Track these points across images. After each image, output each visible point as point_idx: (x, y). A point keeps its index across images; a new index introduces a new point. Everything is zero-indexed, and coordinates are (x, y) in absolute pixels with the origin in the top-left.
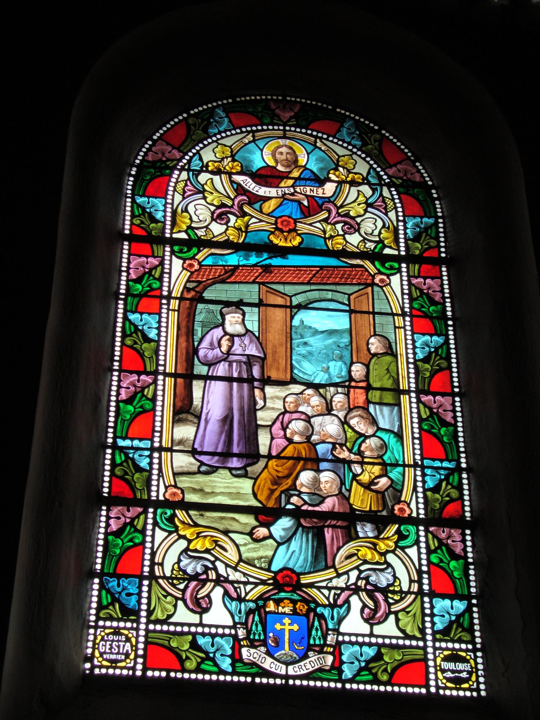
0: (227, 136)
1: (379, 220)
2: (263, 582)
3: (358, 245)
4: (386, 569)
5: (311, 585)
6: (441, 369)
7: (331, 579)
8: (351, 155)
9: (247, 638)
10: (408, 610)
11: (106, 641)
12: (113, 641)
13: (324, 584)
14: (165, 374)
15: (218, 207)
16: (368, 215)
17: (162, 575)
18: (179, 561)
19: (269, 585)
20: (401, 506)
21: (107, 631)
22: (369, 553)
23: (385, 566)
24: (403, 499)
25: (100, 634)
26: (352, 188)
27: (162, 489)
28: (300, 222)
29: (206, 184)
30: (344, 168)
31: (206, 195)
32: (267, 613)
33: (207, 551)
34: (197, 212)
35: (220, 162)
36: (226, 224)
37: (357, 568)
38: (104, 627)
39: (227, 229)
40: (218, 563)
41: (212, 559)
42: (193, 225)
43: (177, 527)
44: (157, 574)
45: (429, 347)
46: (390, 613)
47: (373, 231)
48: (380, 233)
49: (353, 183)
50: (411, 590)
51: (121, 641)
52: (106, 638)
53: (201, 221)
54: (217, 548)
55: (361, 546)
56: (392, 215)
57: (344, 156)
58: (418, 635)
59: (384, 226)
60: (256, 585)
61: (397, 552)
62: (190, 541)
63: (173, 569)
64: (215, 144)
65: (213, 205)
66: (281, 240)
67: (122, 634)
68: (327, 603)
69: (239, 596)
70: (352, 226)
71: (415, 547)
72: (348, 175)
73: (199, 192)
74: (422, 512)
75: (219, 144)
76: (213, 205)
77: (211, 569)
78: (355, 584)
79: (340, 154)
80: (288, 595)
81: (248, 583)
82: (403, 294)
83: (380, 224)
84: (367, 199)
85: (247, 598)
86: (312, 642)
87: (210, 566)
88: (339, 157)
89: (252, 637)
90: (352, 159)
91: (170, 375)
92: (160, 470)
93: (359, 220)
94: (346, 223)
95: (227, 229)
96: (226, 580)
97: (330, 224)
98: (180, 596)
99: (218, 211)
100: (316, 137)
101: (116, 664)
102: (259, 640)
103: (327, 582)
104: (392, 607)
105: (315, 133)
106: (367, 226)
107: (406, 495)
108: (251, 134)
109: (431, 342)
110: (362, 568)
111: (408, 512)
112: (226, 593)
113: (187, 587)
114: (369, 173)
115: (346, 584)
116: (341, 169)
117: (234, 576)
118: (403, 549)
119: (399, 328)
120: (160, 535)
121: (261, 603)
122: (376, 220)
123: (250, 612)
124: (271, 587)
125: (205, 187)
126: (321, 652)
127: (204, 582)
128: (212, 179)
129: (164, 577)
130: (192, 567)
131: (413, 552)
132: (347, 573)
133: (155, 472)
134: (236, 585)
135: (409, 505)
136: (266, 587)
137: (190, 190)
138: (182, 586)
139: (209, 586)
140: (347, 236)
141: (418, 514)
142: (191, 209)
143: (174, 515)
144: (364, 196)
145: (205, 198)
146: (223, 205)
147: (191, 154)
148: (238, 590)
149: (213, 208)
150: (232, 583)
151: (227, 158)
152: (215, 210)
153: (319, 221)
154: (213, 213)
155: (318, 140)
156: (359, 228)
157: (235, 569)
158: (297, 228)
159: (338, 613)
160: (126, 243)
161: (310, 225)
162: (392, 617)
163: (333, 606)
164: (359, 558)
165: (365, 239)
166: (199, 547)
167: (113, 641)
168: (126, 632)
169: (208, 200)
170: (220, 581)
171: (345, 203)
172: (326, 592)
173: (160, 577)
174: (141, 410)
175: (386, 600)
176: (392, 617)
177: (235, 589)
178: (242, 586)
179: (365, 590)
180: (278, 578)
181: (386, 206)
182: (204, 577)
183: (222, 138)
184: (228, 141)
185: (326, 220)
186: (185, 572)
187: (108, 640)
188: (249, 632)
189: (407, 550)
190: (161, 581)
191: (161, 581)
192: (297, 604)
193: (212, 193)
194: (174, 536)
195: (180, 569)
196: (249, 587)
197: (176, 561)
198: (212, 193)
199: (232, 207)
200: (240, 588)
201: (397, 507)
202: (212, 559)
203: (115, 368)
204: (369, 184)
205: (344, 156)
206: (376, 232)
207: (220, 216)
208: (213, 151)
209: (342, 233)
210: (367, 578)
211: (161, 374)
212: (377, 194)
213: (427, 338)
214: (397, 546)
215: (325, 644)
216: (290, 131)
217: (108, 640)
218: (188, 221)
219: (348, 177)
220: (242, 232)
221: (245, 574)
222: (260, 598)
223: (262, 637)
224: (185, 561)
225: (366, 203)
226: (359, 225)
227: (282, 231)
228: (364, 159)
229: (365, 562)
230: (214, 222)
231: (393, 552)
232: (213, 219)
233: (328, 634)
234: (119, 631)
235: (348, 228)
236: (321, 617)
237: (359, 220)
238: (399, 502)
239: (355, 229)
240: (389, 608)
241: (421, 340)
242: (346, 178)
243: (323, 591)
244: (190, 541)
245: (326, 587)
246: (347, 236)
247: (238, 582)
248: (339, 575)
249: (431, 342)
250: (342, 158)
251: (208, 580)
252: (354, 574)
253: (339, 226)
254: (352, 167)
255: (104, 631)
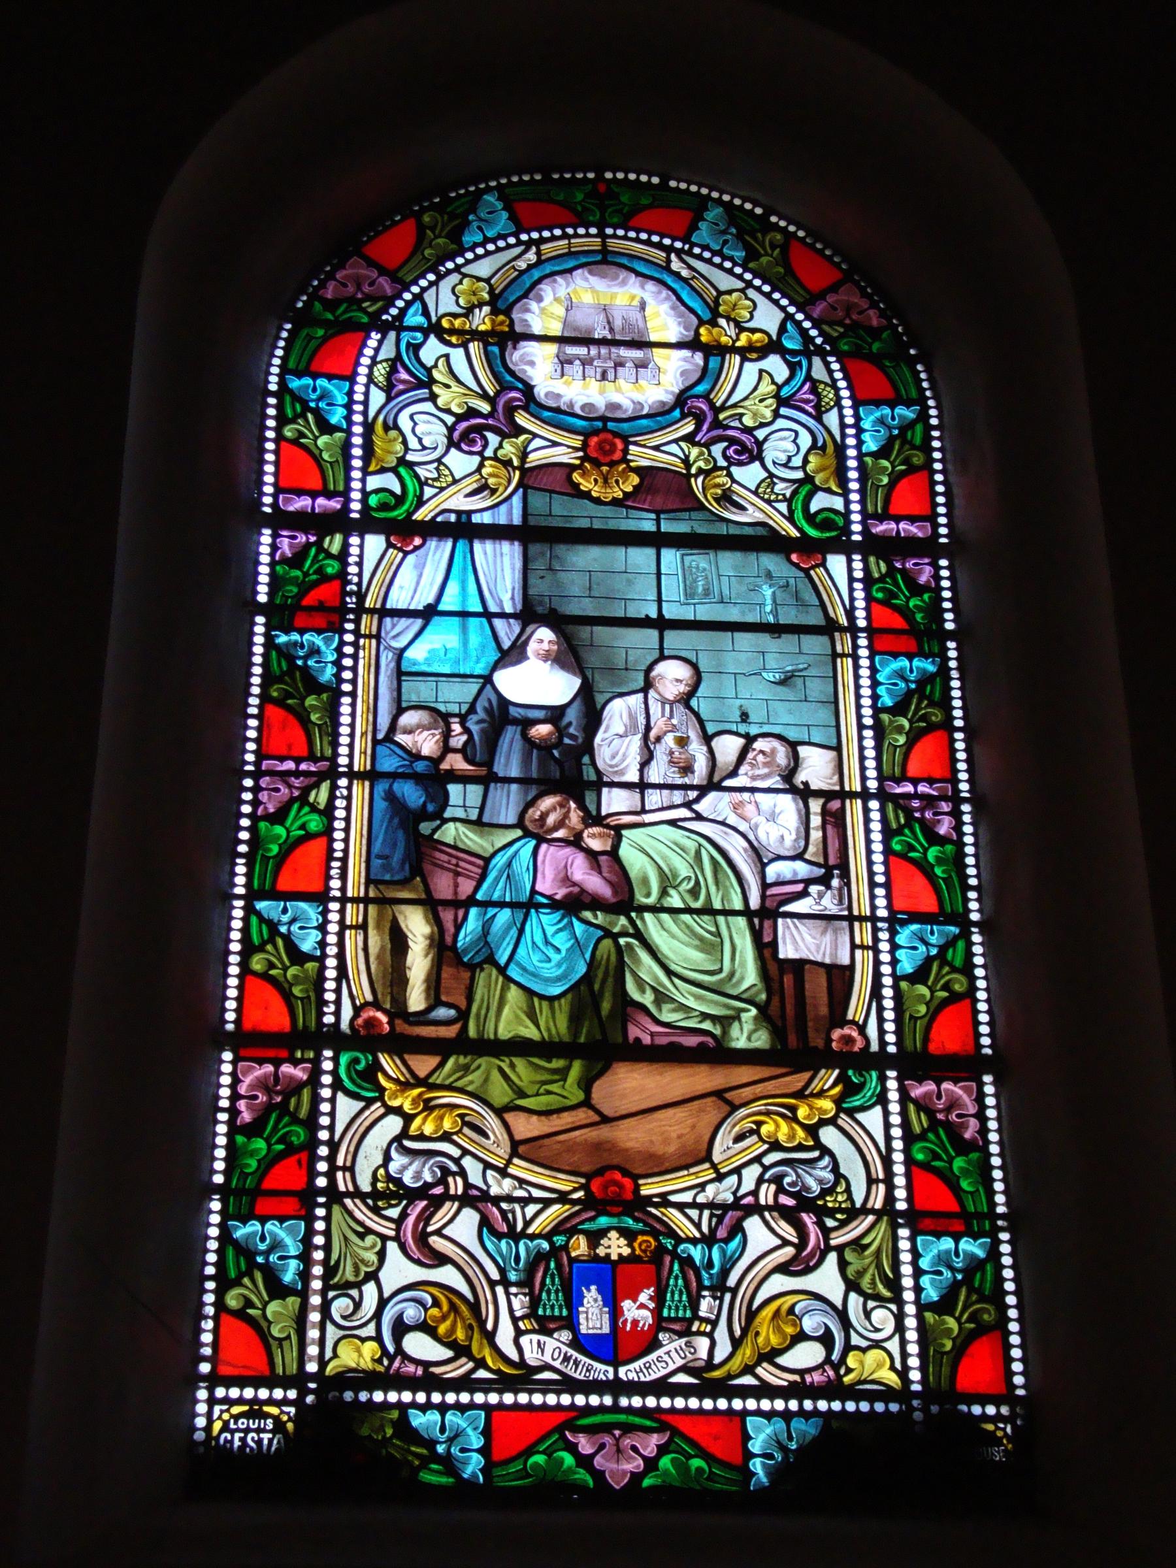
0: (478, 258)
1: (803, 433)
2: (563, 1198)
3: (758, 486)
4: (820, 1158)
5: (664, 1200)
6: (931, 728)
7: (702, 1186)
8: (742, 291)
9: (532, 1314)
10: (866, 1241)
11: (232, 1432)
12: (247, 1431)
13: (687, 1197)
14: (352, 775)
15: (460, 418)
16: (781, 423)
17: (351, 1189)
18: (387, 1158)
19: (574, 1202)
20: (847, 1031)
21: (236, 1410)
22: (784, 1127)
23: (816, 1154)
24: (850, 1016)
25: (220, 1418)
26: (747, 365)
27: (347, 1012)
28: (636, 443)
29: (436, 366)
30: (728, 319)
31: (436, 389)
32: (573, 1261)
33: (446, 1137)
34: (418, 431)
35: (466, 315)
36: (480, 453)
37: (758, 1159)
38: (227, 1401)
39: (481, 466)
40: (467, 1162)
41: (456, 1152)
42: (409, 457)
43: (382, 1090)
44: (342, 1188)
45: (907, 681)
46: (828, 1249)
47: (789, 458)
48: (806, 461)
49: (746, 353)
50: (869, 1205)
51: (264, 1431)
52: (232, 1426)
53: (424, 448)
54: (466, 1130)
55: (768, 1113)
56: (832, 419)
57: (730, 292)
58: (886, 1293)
59: (814, 446)
60: (547, 1203)
61: (840, 1122)
62: (408, 1119)
63: (375, 1179)
64: (454, 278)
65: (448, 411)
66: (596, 480)
67: (267, 1416)
68: (698, 1235)
69: (512, 1226)
70: (744, 449)
71: (878, 1110)
72: (738, 335)
73: (420, 384)
74: (891, 1038)
75: (465, 276)
76: (448, 411)
77: (454, 1174)
78: (755, 1193)
79: (722, 288)
80: (613, 1221)
81: (530, 1200)
82: (851, 580)
83: (805, 440)
84: (780, 388)
85: (530, 1231)
86: (665, 1313)
87: (454, 1168)
88: (720, 293)
89: (540, 1312)
90: (747, 298)
91: (361, 776)
92: (342, 969)
93: (760, 434)
94: (732, 441)
95: (481, 466)
96: (485, 1196)
97: (698, 444)
98: (392, 1233)
99: (464, 425)
100: (669, 250)
101: (251, 1409)
102: (560, 1318)
103: (693, 1192)
104: (833, 1235)
105: (667, 242)
106: (777, 449)
107: (856, 1008)
108: (534, 249)
109: (911, 671)
110: (768, 1160)
111: (859, 1044)
112: (485, 1222)
113: (404, 1215)
114: (782, 329)
115: (734, 1193)
116: (722, 322)
117: (499, 1187)
118: (851, 1113)
119: (843, 655)
120: (346, 1107)
121: (559, 1240)
122: (796, 433)
123: (539, 1258)
124: (577, 1208)
125: (435, 374)
126: (686, 1333)
127: (437, 1203)
128: (447, 356)
129: (357, 1194)
130: (411, 1173)
131: (873, 1119)
132: (737, 1171)
133: (331, 962)
134: (504, 1206)
135: (862, 1029)
136: (567, 1207)
137: (404, 382)
138: (394, 1213)
139: (449, 1208)
140: (734, 469)
141: (883, 1043)
142: (404, 422)
143: (376, 1067)
144: (773, 382)
145: (433, 398)
146: (472, 413)
147: (400, 304)
148: (510, 1216)
149: (450, 420)
150: (496, 1201)
151: (480, 305)
152: (455, 424)
153: (676, 441)
154: (451, 429)
155: (673, 256)
156: (760, 451)
157: (503, 1173)
158: (629, 457)
159: (723, 1252)
160: (267, 531)
161: (657, 448)
162: (832, 1257)
163: (709, 1240)
164: (761, 1139)
165: (771, 475)
166: (428, 1129)
167: (247, 1431)
168: (274, 1410)
169: (440, 402)
170: (473, 1198)
171: (729, 403)
172: (693, 1213)
173: (347, 1194)
174: (302, 832)
175: (820, 1224)
176: (832, 1257)
177: (503, 1213)
178: (517, 1207)
179: (777, 1207)
180: (595, 1186)
181: (819, 399)
182: (438, 1190)
183: (468, 262)
184: (483, 268)
185: (689, 438)
186: (398, 1182)
187: (238, 1430)
188: (535, 1302)
189: (860, 1116)
190: (348, 1201)
191: (348, 1201)
192: (635, 1239)
193: (448, 386)
194: (377, 1109)
195: (389, 1178)
196: (531, 1209)
197: (380, 1162)
198: (448, 386)
199: (491, 415)
200: (513, 1212)
201: (836, 1034)
202: (456, 1152)
203: (243, 861)
204: (783, 352)
205: (730, 292)
206: (797, 461)
207: (465, 436)
208: (453, 293)
209: (725, 464)
210: (778, 1180)
211: (343, 774)
212: (801, 376)
213: (903, 662)
214: (839, 1109)
215: (696, 1316)
216: (615, 236)
217: (238, 1430)
218: (399, 447)
219: (738, 339)
220: (514, 468)
221: (522, 1182)
222: (556, 1230)
223: (565, 1313)
224: (398, 1161)
225: (777, 396)
226: (760, 444)
227: (597, 464)
228: (768, 296)
229: (775, 1146)
230: (453, 450)
231: (832, 1121)
232: (451, 444)
233: (700, 1297)
234: (260, 1409)
235: (736, 452)
236: (688, 1261)
237: (760, 434)
238: (843, 1022)
239: (750, 451)
240: (827, 1239)
241: (890, 667)
242: (734, 342)
243: (688, 1211)
244: (408, 1119)
245: (694, 1205)
246: (734, 469)
247: (509, 1199)
248: (720, 1177)
249: (911, 671)
250: (727, 297)
251: (446, 1197)
252: (751, 1174)
253: (717, 449)
254: (748, 316)
255: (228, 1411)
